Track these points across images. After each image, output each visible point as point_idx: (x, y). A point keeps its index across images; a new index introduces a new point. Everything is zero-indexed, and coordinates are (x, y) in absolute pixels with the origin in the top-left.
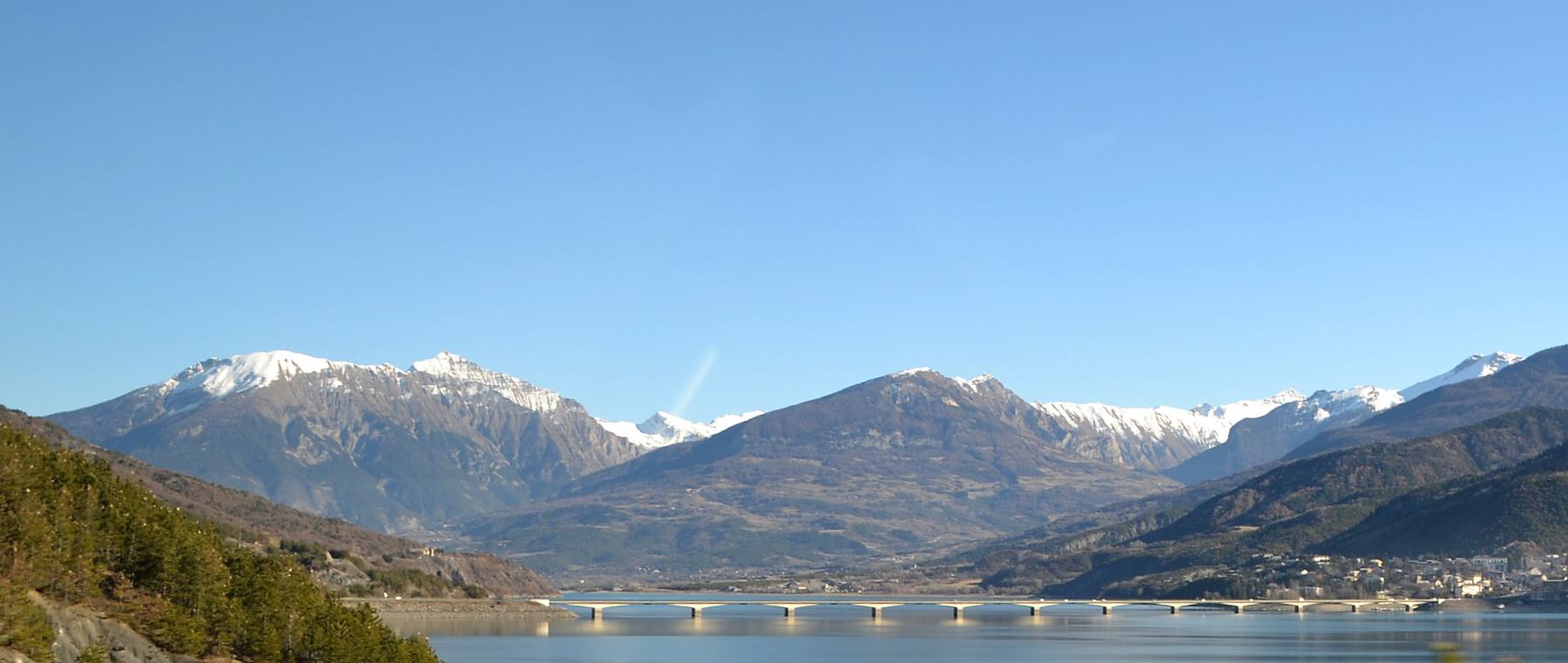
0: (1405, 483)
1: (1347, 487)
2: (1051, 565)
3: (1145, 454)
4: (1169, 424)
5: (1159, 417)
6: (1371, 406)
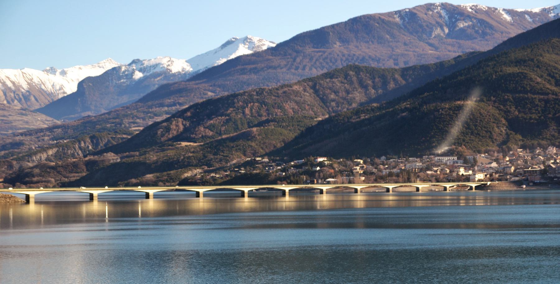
0: (281, 114)
1: (245, 117)
2: (59, 169)
3: (17, 99)
4: (31, 80)
5: (24, 75)
6: (169, 69)
